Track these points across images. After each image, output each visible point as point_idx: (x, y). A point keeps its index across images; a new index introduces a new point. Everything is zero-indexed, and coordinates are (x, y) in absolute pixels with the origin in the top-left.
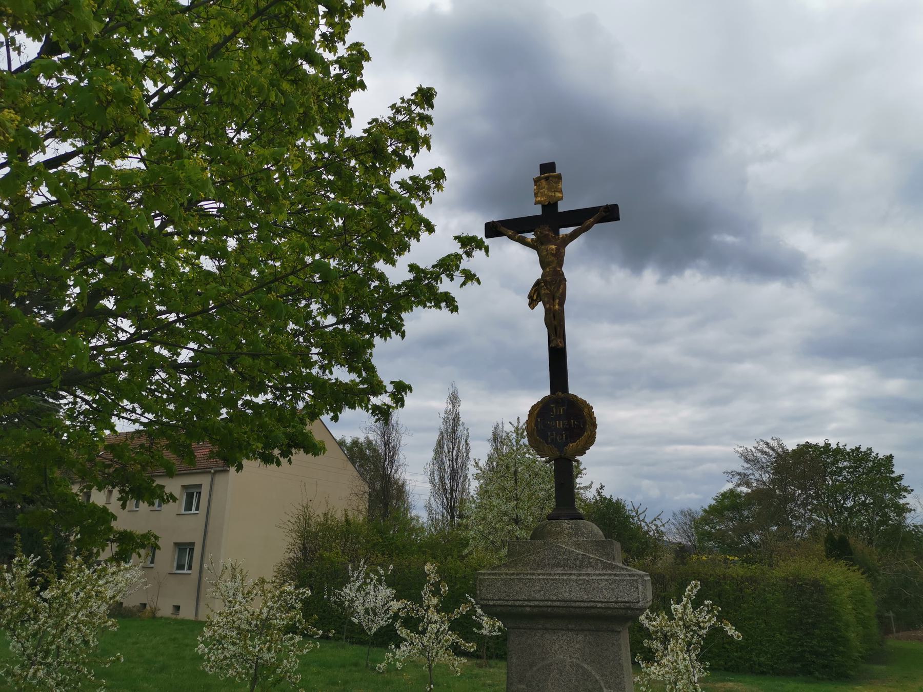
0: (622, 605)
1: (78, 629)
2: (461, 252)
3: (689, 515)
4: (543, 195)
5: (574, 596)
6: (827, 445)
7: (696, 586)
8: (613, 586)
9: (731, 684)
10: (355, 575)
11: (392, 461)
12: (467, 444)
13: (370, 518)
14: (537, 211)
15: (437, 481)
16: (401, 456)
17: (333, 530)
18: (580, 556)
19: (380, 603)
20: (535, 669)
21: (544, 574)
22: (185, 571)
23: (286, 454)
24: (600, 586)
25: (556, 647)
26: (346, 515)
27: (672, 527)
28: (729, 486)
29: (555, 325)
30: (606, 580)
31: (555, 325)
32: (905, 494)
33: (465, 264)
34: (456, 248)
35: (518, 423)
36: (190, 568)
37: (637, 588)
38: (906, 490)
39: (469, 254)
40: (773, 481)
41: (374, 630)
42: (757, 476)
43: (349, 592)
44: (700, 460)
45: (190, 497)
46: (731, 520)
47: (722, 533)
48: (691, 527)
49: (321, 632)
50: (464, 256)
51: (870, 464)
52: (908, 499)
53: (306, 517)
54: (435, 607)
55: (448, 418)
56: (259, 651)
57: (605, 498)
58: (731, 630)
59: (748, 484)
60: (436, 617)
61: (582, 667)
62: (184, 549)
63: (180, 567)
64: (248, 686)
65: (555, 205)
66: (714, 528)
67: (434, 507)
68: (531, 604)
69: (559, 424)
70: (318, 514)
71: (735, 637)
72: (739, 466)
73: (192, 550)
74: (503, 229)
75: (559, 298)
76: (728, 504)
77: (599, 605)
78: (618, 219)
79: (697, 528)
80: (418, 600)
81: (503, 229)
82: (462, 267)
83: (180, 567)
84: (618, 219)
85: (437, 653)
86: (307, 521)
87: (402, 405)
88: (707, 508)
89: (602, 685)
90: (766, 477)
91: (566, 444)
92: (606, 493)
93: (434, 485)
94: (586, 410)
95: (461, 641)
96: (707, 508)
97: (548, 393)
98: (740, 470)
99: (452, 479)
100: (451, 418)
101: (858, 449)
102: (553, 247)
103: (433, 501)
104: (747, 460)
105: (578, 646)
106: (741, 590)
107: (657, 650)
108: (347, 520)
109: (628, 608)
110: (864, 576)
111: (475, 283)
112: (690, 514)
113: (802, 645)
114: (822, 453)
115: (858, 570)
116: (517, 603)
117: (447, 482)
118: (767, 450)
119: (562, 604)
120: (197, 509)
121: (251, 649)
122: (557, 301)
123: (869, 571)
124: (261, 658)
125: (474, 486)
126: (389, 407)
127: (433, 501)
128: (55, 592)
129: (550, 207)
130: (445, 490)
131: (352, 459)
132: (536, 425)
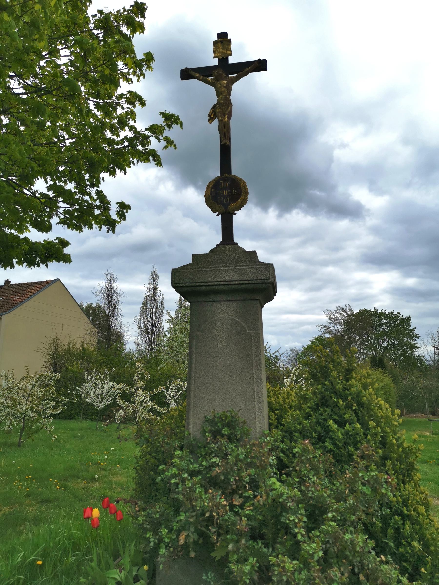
0: (260, 281)
2: (164, 124)
4: (219, 52)
5: (231, 278)
6: (376, 310)
7: (299, 367)
8: (255, 271)
10: (89, 378)
11: (113, 314)
12: (162, 304)
13: (99, 347)
14: (215, 62)
15: (143, 327)
16: (120, 311)
17: (74, 354)
18: (236, 257)
19: (105, 391)
20: (207, 323)
21: (214, 268)
24: (247, 272)
25: (220, 311)
26: (83, 345)
27: (285, 358)
28: (318, 334)
29: (225, 132)
30: (251, 268)
31: (225, 132)
32: (416, 339)
33: (167, 133)
34: (160, 121)
37: (269, 271)
38: (417, 337)
39: (169, 127)
40: (344, 331)
41: (101, 407)
43: (86, 387)
44: (301, 324)
48: (296, 358)
49: (67, 399)
50: (166, 127)
51: (398, 321)
53: (55, 344)
54: (141, 387)
55: (150, 288)
56: (25, 410)
59: (330, 332)
60: (142, 393)
61: (234, 320)
64: (19, 434)
65: (227, 59)
67: (140, 343)
68: (206, 284)
69: (225, 192)
70: (64, 342)
74: (193, 73)
75: (228, 114)
76: (319, 342)
77: (246, 282)
78: (267, 70)
79: (299, 358)
80: (130, 383)
82: (165, 135)
84: (267, 70)
85: (142, 414)
86: (56, 347)
87: (124, 219)
88: (306, 347)
89: (246, 328)
90: (340, 328)
91: (229, 204)
93: (141, 329)
94: (242, 184)
95: (157, 407)
96: (306, 347)
97: (219, 174)
99: (152, 326)
100: (152, 287)
101: (392, 312)
102: (225, 82)
105: (233, 309)
108: (84, 349)
109: (263, 283)
110: (391, 379)
111: (173, 148)
112: (295, 351)
114: (372, 315)
115: (388, 375)
116: (197, 284)
117: (149, 327)
119: (224, 283)
121: (21, 410)
122: (226, 116)
123: (395, 379)
124: (27, 415)
125: (166, 326)
129: (223, 60)
130: (147, 332)
131: (88, 315)
132: (211, 194)
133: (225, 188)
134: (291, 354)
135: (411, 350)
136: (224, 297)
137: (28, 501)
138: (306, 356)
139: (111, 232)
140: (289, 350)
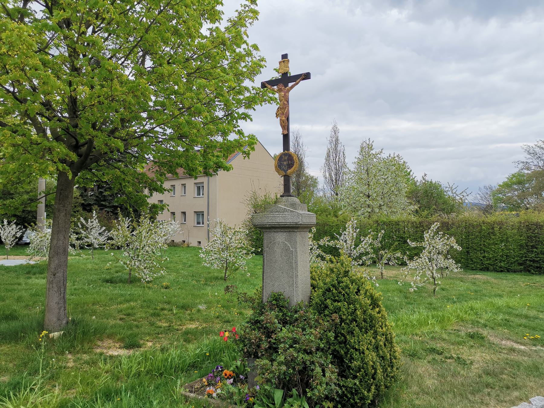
1: (149, 247)
9: (478, 276)
12: (344, 155)
22: (201, 225)
23: (215, 171)
27: (478, 195)
28: (515, 171)
29: (285, 125)
35: (369, 141)
36: (203, 223)
42: (536, 163)
45: (199, 188)
46: (516, 190)
47: (510, 198)
49: (254, 249)
57: (428, 181)
62: (199, 214)
63: (198, 223)
69: (285, 163)
71: (458, 249)
73: (203, 215)
76: (518, 181)
79: (494, 196)
83: (198, 223)
92: (428, 178)
93: (326, 178)
96: (502, 184)
97: (282, 151)
99: (336, 174)
100: (334, 140)
102: (283, 93)
103: (325, 187)
104: (530, 153)
106: (493, 228)
113: (526, 257)
117: (334, 176)
120: (203, 195)
127: (325, 187)
128: (138, 232)
129: (285, 75)
130: (332, 181)
133: (285, 160)
134: (484, 191)
136: (279, 230)
137: (217, 321)
138: (501, 193)
139: (246, 158)
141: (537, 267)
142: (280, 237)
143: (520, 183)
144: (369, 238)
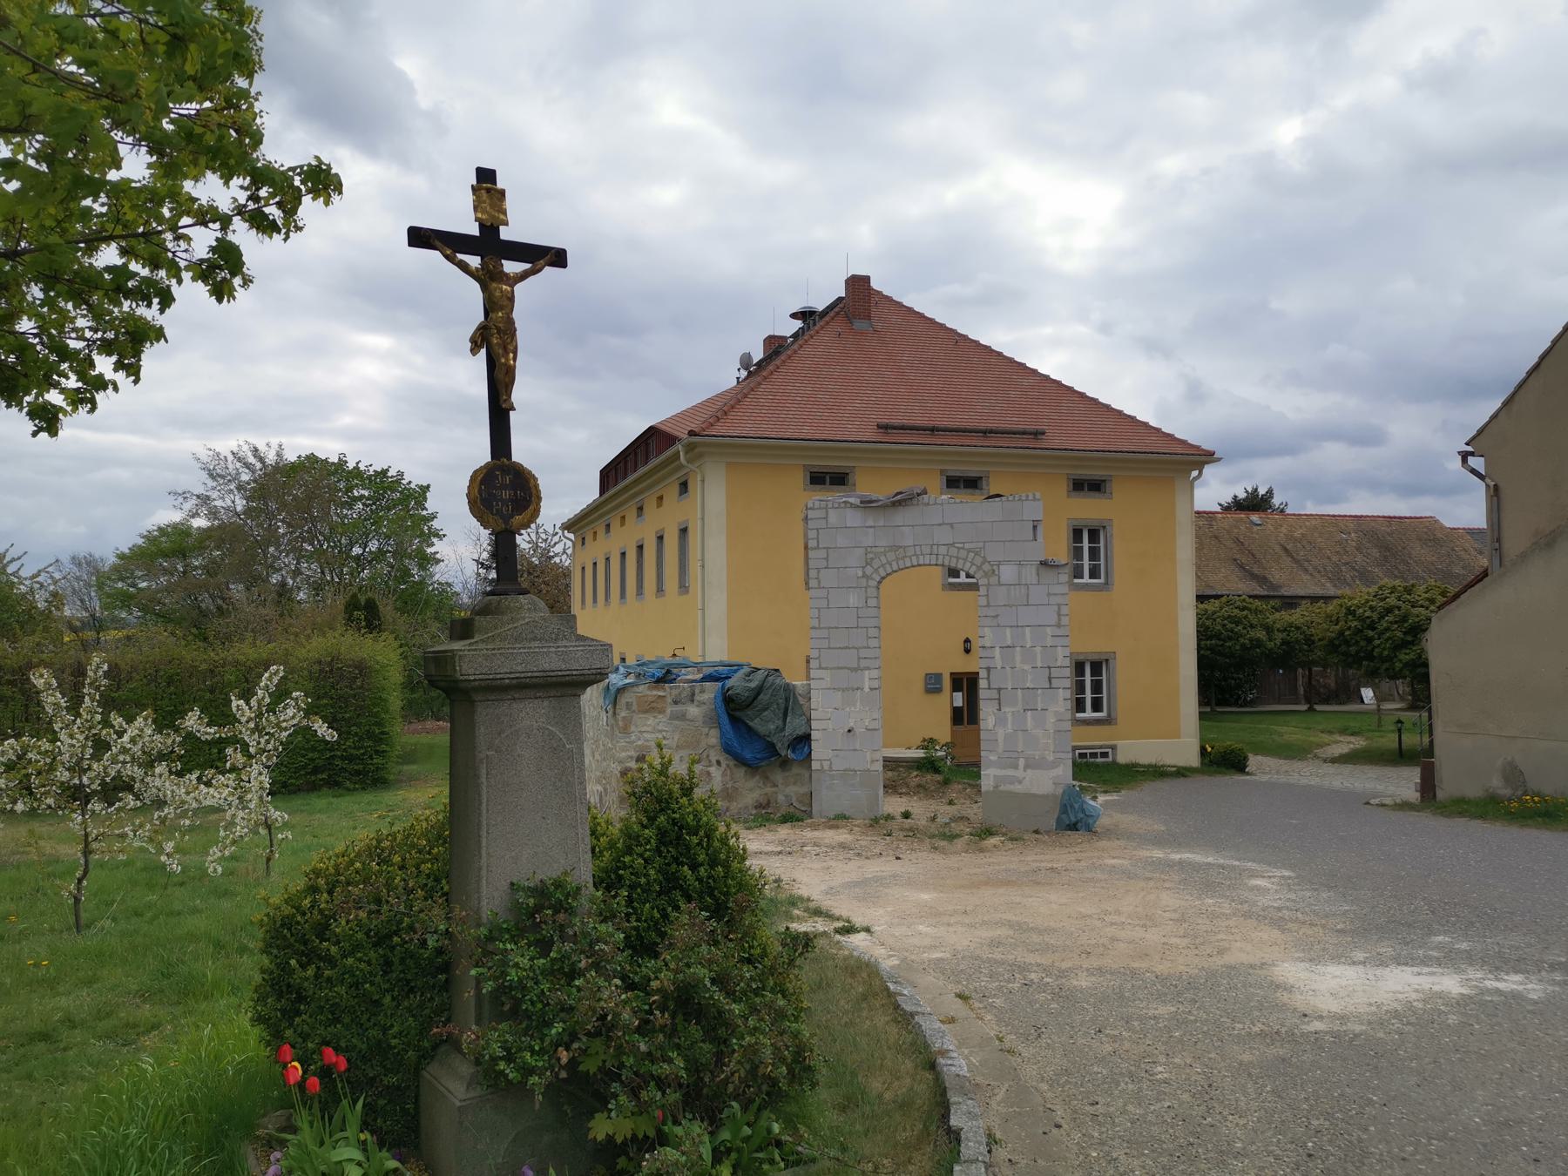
3: (88, 563)
6: (342, 463)
14: (474, 230)
28: (176, 517)
32: (435, 540)
38: (437, 535)
40: (248, 511)
46: (165, 571)
48: (88, 585)
52: (438, 547)
58: (321, 728)
66: (134, 586)
69: (506, 494)
72: (198, 483)
76: (169, 546)
78: (564, 266)
79: (100, 586)
81: (438, 243)
98: (200, 490)
101: (384, 472)
104: (212, 476)
107: (133, 779)
118: (251, 460)
126: (59, 409)
129: (490, 229)
132: (480, 491)
133: (503, 487)
135: (422, 567)
138: (122, 579)
140: (65, 559)
141: (358, 773)
142: (531, 715)
143: (182, 553)
144: (146, 719)
